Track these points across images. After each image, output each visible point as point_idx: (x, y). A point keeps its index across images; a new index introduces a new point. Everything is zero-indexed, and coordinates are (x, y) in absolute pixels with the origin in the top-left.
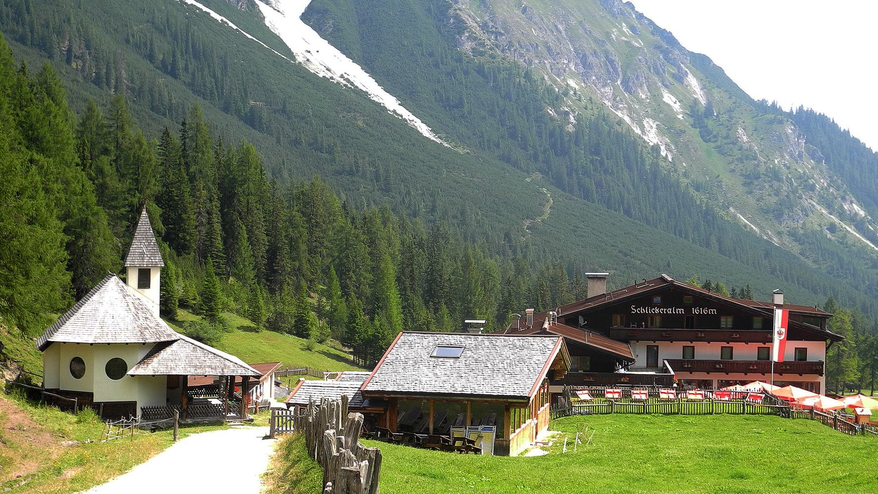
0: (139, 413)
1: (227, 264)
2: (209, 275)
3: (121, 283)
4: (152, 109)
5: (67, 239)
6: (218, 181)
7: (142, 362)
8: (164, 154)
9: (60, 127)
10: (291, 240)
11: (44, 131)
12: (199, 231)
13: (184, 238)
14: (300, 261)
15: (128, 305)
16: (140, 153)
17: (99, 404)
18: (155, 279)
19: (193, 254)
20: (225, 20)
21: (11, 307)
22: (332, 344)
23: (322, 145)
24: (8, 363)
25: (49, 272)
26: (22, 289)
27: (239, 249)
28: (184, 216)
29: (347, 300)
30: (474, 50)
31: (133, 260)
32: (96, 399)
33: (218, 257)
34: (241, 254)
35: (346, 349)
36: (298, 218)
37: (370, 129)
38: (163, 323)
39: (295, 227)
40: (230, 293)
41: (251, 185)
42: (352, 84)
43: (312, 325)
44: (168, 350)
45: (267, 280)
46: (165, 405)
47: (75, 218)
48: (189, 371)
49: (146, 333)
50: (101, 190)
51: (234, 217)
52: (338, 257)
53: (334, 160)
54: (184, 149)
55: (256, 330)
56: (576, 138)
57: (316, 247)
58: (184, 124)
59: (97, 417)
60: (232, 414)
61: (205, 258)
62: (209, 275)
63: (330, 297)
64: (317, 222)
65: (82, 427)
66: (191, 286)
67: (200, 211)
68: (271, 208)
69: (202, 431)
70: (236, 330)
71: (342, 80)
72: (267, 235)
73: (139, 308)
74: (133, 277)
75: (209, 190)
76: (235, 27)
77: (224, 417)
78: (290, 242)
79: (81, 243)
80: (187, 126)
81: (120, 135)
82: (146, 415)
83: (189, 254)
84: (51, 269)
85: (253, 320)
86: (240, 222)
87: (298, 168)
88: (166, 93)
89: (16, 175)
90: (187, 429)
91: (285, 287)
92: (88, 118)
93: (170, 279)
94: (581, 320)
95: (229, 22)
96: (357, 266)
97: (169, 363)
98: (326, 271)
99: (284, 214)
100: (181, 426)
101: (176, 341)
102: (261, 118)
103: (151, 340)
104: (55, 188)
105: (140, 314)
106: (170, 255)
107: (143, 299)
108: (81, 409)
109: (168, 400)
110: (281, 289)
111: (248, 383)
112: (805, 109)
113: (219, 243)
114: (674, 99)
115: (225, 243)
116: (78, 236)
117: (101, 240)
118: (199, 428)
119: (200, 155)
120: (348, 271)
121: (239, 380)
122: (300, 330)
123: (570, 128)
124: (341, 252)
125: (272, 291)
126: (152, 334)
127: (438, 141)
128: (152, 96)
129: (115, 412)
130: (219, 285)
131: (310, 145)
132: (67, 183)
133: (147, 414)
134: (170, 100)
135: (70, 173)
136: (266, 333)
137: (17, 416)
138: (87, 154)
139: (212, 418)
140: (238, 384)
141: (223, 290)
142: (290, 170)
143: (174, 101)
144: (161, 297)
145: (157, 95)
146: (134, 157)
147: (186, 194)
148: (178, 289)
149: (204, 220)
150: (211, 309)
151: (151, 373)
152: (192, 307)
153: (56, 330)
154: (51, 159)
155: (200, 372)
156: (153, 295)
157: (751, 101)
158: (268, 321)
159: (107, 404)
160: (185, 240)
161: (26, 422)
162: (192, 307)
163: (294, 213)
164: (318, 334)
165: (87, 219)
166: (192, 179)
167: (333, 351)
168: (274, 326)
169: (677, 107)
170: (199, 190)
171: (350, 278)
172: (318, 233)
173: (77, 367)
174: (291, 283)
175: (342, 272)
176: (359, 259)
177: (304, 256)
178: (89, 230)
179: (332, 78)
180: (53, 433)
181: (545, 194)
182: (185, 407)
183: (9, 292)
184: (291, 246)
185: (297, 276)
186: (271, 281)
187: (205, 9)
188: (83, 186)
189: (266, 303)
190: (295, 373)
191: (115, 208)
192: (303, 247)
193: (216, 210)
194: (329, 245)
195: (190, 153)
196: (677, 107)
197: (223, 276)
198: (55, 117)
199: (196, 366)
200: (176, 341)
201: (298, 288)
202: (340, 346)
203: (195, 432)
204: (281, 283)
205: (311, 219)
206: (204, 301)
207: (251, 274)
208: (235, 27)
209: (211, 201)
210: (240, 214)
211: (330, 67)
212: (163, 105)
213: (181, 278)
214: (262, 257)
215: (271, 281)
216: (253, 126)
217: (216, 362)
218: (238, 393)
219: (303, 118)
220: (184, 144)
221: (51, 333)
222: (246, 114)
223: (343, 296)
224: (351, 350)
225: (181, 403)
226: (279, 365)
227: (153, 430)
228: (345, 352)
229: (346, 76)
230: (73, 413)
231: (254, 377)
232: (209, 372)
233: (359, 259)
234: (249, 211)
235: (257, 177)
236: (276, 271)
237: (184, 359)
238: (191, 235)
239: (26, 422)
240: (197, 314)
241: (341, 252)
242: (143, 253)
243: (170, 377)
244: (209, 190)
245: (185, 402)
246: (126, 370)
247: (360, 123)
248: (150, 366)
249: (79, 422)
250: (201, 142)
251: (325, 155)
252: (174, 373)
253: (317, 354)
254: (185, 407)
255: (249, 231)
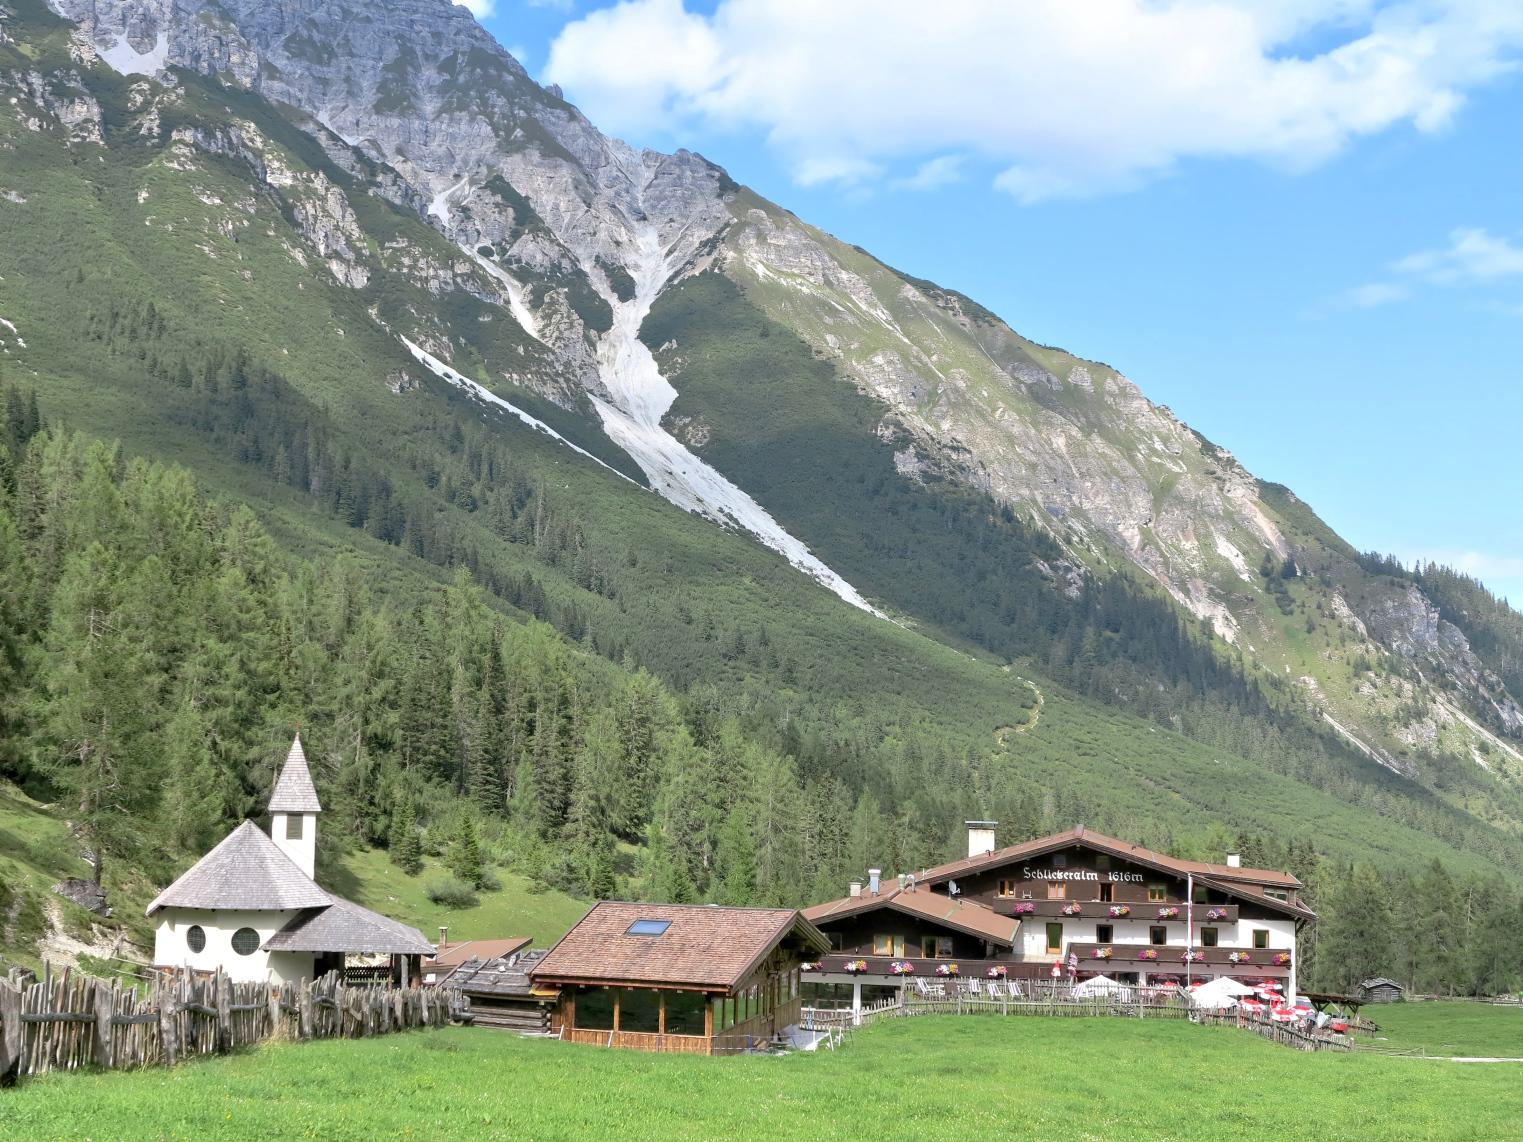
20: (542, 425)
30: (924, 474)
42: (736, 521)
56: (1084, 607)
71: (720, 515)
76: (557, 436)
94: (953, 888)
95: (547, 428)
112: (1438, 567)
114: (1236, 551)
123: (1073, 592)
127: (868, 608)
151: (289, 949)
157: (1357, 558)
169: (1238, 562)
179: (705, 513)
181: (1032, 690)
187: (512, 409)
196: (1238, 562)
208: (557, 436)
211: (702, 496)
229: (727, 510)
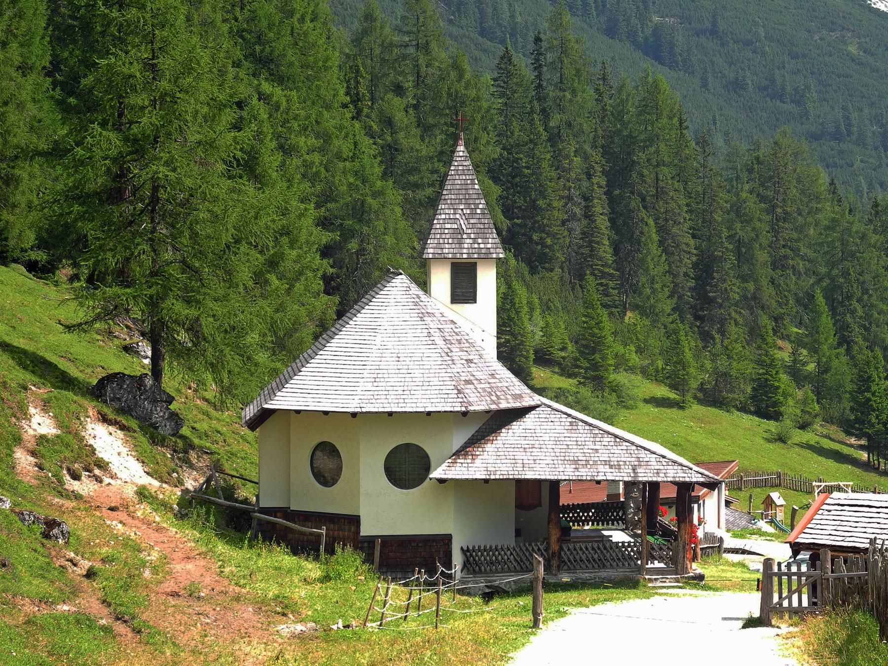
0: (457, 559)
1: (619, 288)
2: (588, 305)
3: (415, 290)
4: (482, 33)
5: (326, 237)
6: (601, 141)
7: (462, 452)
8: (502, 95)
9: (311, 38)
10: (739, 243)
11: (282, 45)
12: (570, 230)
13: (542, 242)
14: (756, 281)
15: (429, 335)
16: (460, 87)
17: (371, 540)
18: (487, 281)
19: (558, 270)
21: (195, 345)
22: (825, 432)
23: (783, 89)
24: (193, 455)
25: (289, 291)
26: (217, 308)
27: (643, 261)
28: (541, 203)
29: (848, 351)
31: (439, 246)
32: (366, 530)
33: (604, 275)
34: (647, 270)
35: (853, 441)
36: (752, 204)
37: (871, 60)
38: (505, 373)
39: (746, 220)
40: (626, 336)
41: (662, 146)
43: (785, 395)
44: (517, 427)
45: (697, 317)
46: (512, 543)
47: (342, 201)
48: (564, 472)
49: (469, 390)
50: (390, 153)
51: (633, 204)
52: (828, 275)
53: (806, 114)
54: (540, 86)
55: (679, 405)
57: (785, 257)
58: (538, 40)
59: (365, 567)
60: (657, 565)
61: (581, 277)
62: (588, 305)
63: (814, 350)
64: (786, 213)
65: (332, 592)
66: (557, 326)
67: (571, 186)
68: (700, 189)
69: (594, 602)
70: (641, 404)
72: (694, 236)
73: (455, 340)
74: (441, 280)
75: (586, 158)
77: (640, 570)
78: (738, 249)
79: (353, 245)
80: (544, 45)
81: (422, 60)
82: (472, 564)
83: (552, 270)
84: (292, 286)
85: (673, 387)
86: (643, 214)
87: (740, 131)
88: (505, 6)
89: (198, 78)
90: (562, 596)
91: (733, 329)
92: (365, 32)
93: (518, 313)
96: (865, 291)
97: (520, 455)
98: (807, 301)
99: (724, 199)
100: (550, 587)
101: (538, 406)
102: (672, 46)
103: (479, 405)
104: (302, 144)
105: (456, 353)
106: (517, 271)
107: (464, 326)
108: (331, 551)
109: (518, 533)
110: (722, 332)
111: (686, 496)
113: (606, 251)
115: (616, 251)
116: (347, 234)
117: (390, 240)
118: (588, 595)
119: (568, 95)
120: (849, 298)
121: (670, 493)
122: (764, 405)
124: (833, 265)
125: (706, 337)
126: (480, 393)
128: (482, 12)
129: (408, 558)
130: (608, 325)
131: (762, 89)
132: (326, 137)
133: (474, 562)
134: (513, 17)
135: (330, 121)
136: (697, 409)
137: (190, 566)
138: (362, 90)
139: (620, 575)
140: (668, 502)
141: (615, 334)
142: (726, 134)
143: (519, 19)
144: (499, 346)
145: (490, 10)
146: (449, 95)
147: (545, 165)
148: (534, 330)
149: (577, 211)
150: (595, 367)
152: (559, 364)
153: (281, 386)
154: (294, 93)
155: (585, 473)
156: (481, 319)
158: (701, 388)
159: (388, 541)
160: (544, 245)
161: (208, 580)
162: (559, 364)
163: (744, 195)
164: (798, 412)
165: (363, 202)
166: (554, 138)
167: (827, 444)
168: (713, 398)
170: (567, 157)
171: (853, 312)
172: (788, 232)
173: (326, 463)
174: (740, 320)
175: (838, 301)
176: (867, 277)
177: (765, 273)
178: (368, 222)
180: (261, 604)
182: (555, 547)
183: (192, 312)
184: (739, 255)
185: (751, 308)
186: (701, 319)
188: (356, 144)
189: (697, 357)
190: (757, 484)
191: (416, 186)
192: (762, 257)
193: (599, 192)
194: (811, 254)
195: (551, 92)
197: (617, 309)
198: (302, 20)
199: (576, 462)
200: (538, 406)
201: (754, 333)
202: (842, 436)
203: (580, 604)
204: (723, 322)
205: (774, 207)
206: (581, 352)
207: (667, 306)
209: (589, 176)
210: (643, 200)
212: (500, 25)
213: (538, 311)
214: (686, 275)
215: (701, 319)
216: (659, 59)
217: (619, 453)
218: (668, 518)
219: (747, 43)
220: (539, 77)
221: (272, 394)
222: (646, 39)
223: (840, 345)
224: (863, 442)
225: (547, 539)
226: (733, 468)
227: (488, 597)
228: (851, 446)
230: (317, 558)
231: (703, 485)
232: (605, 473)
233: (867, 277)
234: (660, 193)
235: (673, 132)
236: (711, 301)
237: (550, 445)
238: (554, 236)
239: (208, 580)
240: (570, 376)
241: (833, 265)
242: (459, 231)
243: (521, 484)
244: (586, 158)
245: (554, 538)
246: (427, 469)
247: (853, 49)
248: (478, 462)
249: (326, 578)
250: (569, 72)
251: (790, 107)
252: (530, 475)
253: (797, 449)
254: (555, 547)
255: (662, 230)
